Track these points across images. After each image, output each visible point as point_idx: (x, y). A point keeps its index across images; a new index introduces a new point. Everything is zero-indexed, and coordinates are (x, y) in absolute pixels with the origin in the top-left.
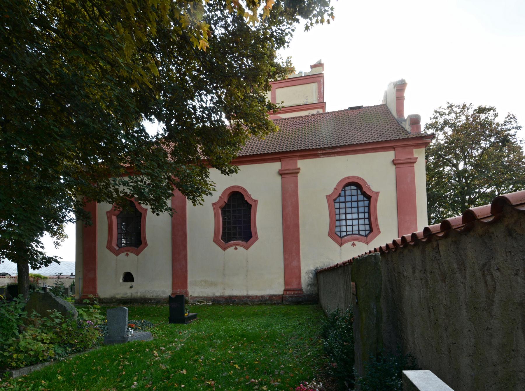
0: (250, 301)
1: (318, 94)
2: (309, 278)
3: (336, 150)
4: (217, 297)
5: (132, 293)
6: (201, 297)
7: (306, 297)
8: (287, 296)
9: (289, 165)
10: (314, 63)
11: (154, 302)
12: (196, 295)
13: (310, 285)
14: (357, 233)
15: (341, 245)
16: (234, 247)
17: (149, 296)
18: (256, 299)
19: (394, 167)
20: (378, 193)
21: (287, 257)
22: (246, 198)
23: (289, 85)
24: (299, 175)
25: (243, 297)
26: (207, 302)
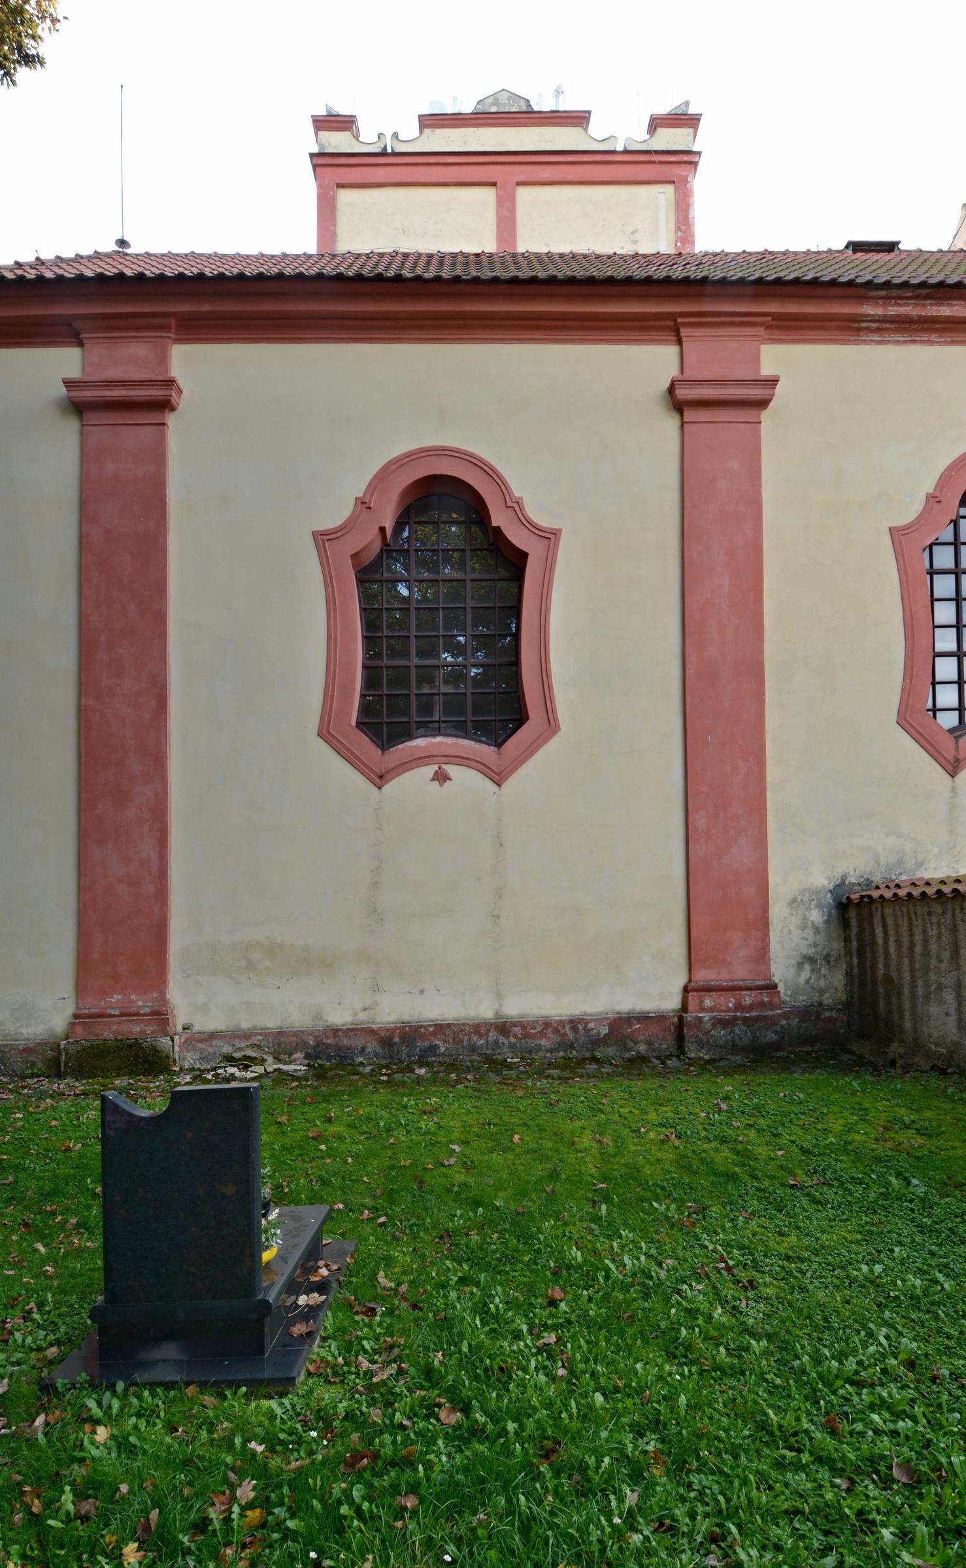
0: (511, 1046)
1: (678, 229)
2: (803, 926)
3: (945, 311)
4: (336, 1031)
6: (246, 1036)
7: (795, 1022)
8: (706, 1016)
10: (664, 108)
12: (214, 1022)
13: (810, 960)
16: (430, 770)
18: (542, 1034)
21: (700, 821)
22: (498, 518)
23: (570, 178)
25: (478, 1028)
26: (277, 1059)
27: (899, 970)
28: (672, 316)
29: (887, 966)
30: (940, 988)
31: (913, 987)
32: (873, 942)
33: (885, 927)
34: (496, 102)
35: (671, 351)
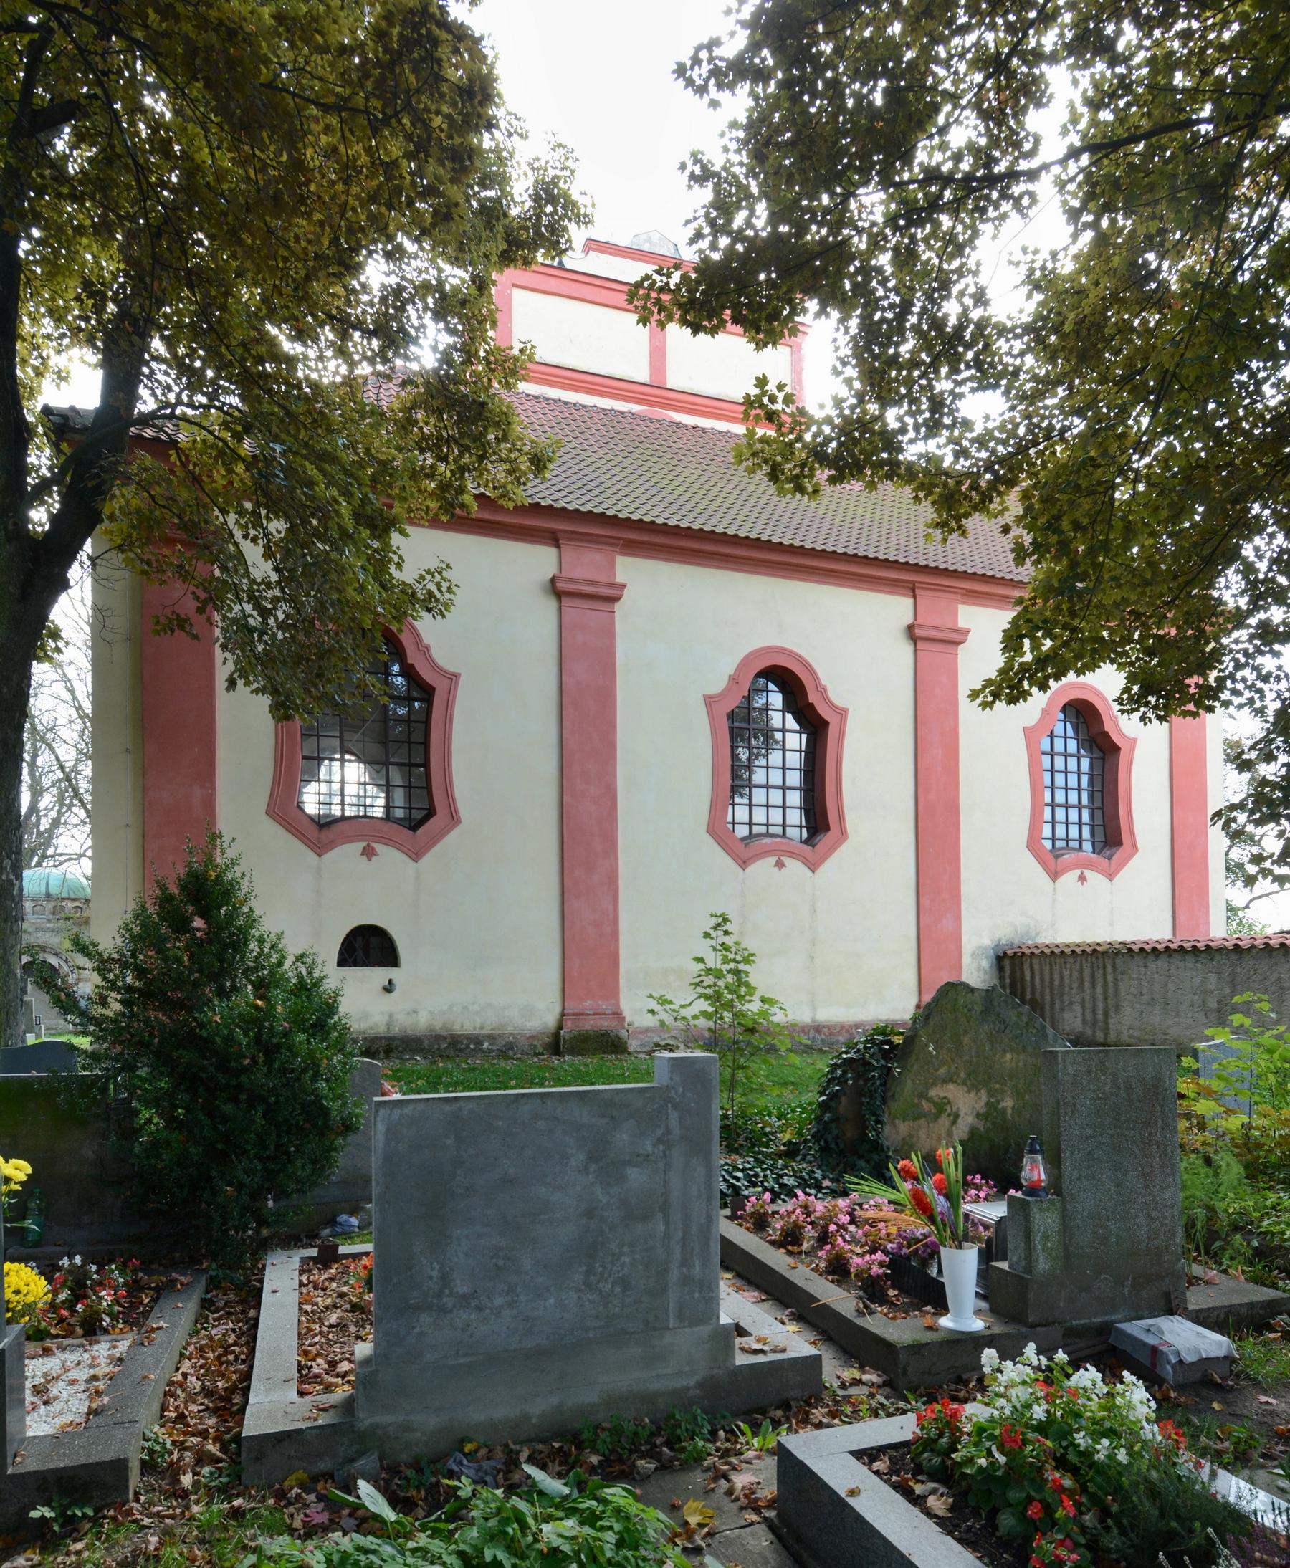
2: (978, 969)
5: (391, 1016)
9: (935, 607)
11: (491, 1051)
14: (779, 830)
15: (744, 863)
16: (773, 860)
17: (466, 1024)
19: (552, 604)
20: (1134, 741)
24: (618, 607)
27: (1042, 995)
28: (914, 583)
29: (1033, 993)
30: (1071, 1003)
31: (1052, 1008)
32: (1023, 979)
33: (1032, 970)
34: (649, 240)
35: (907, 602)
